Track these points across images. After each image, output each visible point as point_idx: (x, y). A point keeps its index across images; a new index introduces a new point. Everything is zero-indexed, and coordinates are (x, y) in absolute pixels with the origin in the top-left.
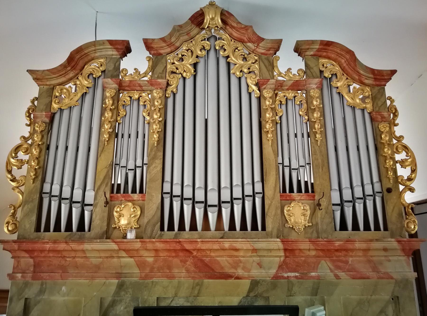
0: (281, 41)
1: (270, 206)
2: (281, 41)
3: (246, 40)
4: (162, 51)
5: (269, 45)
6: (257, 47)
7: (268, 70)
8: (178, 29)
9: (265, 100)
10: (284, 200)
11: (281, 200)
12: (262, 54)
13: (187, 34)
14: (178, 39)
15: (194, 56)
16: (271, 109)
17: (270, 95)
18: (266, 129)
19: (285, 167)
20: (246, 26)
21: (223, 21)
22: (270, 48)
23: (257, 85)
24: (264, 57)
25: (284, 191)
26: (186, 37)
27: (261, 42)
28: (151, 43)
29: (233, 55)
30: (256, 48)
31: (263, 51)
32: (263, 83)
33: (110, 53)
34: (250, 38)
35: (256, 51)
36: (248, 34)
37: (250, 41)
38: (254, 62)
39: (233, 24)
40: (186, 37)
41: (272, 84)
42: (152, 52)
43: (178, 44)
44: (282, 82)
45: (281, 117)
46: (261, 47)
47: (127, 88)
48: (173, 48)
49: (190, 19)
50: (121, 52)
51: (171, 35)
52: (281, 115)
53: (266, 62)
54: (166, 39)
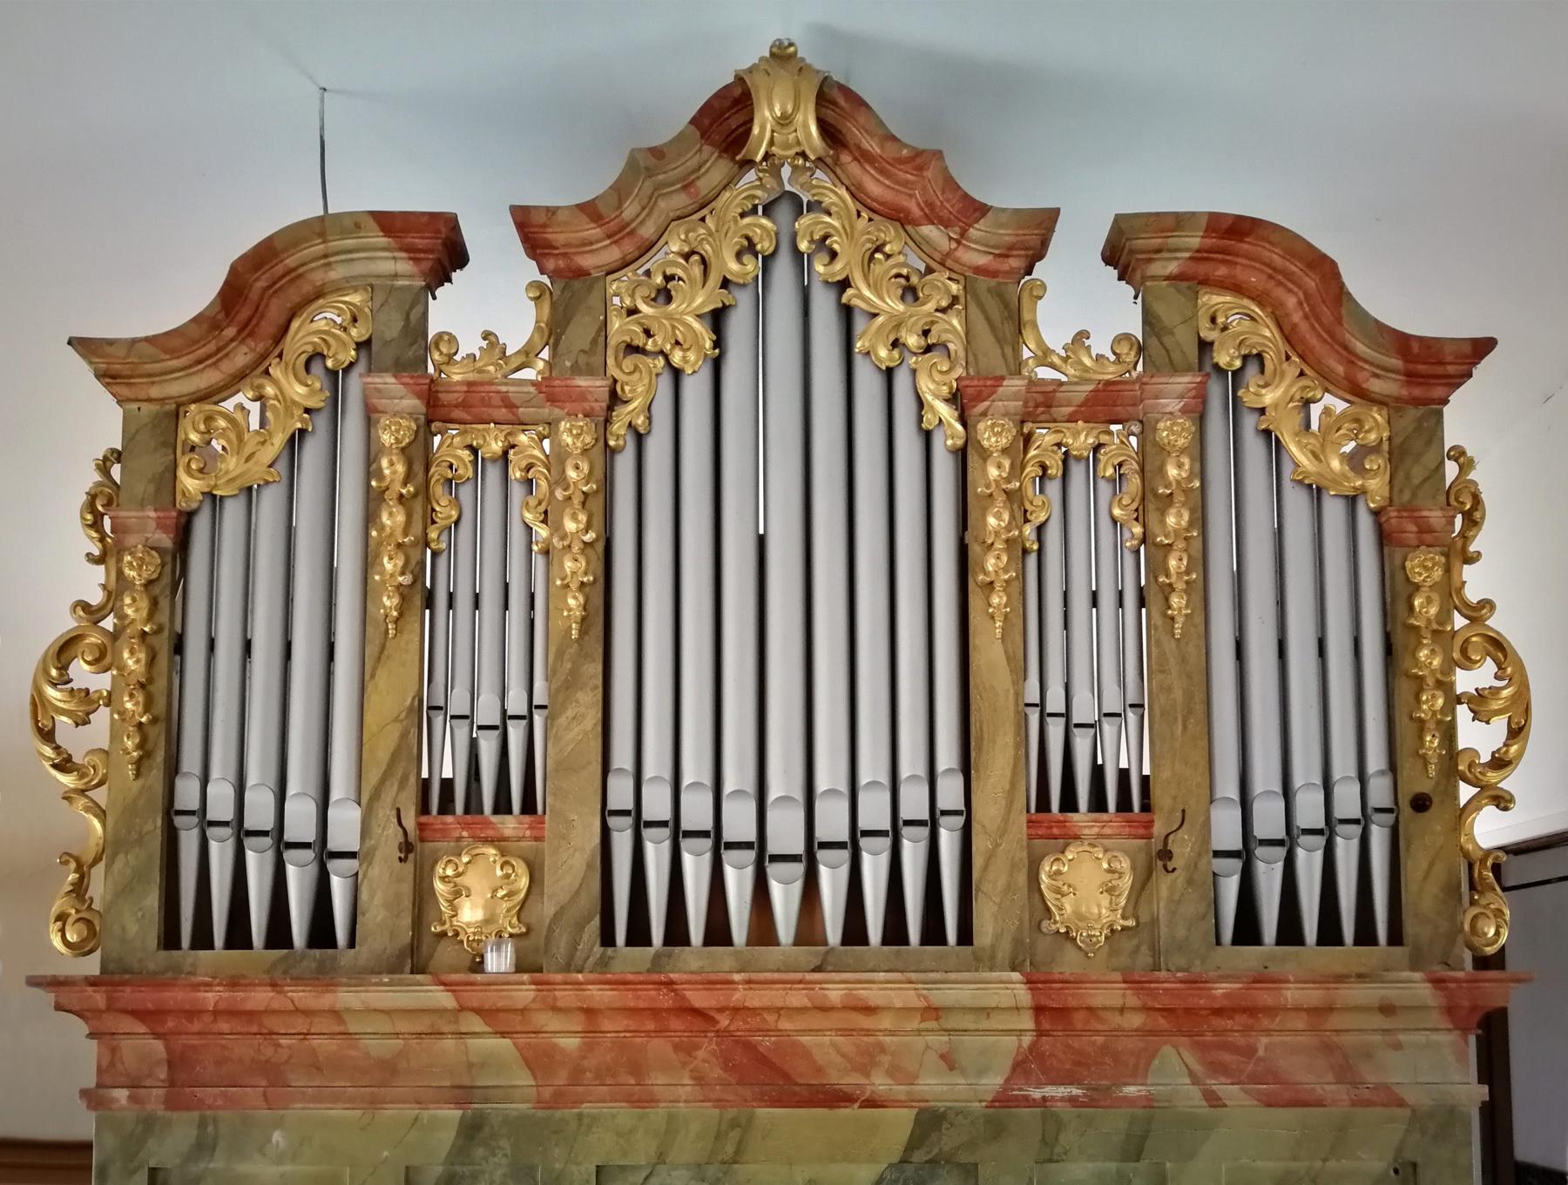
4: (587, 261)
5: (1007, 235)
6: (959, 242)
7: (998, 340)
9: (985, 460)
10: (1041, 837)
11: (1030, 837)
12: (978, 270)
13: (685, 187)
15: (714, 279)
16: (1004, 497)
17: (1004, 442)
18: (986, 573)
20: (918, 153)
22: (1011, 247)
24: (984, 283)
26: (680, 201)
27: (977, 221)
28: (544, 226)
29: (866, 277)
30: (954, 245)
31: (983, 261)
32: (980, 393)
33: (386, 267)
34: (931, 205)
36: (924, 189)
37: (932, 216)
38: (944, 303)
39: (866, 146)
41: (1014, 397)
42: (551, 264)
43: (648, 231)
44: (1050, 388)
45: (1040, 529)
48: (629, 247)
49: (694, 121)
53: (993, 305)
54: (602, 209)
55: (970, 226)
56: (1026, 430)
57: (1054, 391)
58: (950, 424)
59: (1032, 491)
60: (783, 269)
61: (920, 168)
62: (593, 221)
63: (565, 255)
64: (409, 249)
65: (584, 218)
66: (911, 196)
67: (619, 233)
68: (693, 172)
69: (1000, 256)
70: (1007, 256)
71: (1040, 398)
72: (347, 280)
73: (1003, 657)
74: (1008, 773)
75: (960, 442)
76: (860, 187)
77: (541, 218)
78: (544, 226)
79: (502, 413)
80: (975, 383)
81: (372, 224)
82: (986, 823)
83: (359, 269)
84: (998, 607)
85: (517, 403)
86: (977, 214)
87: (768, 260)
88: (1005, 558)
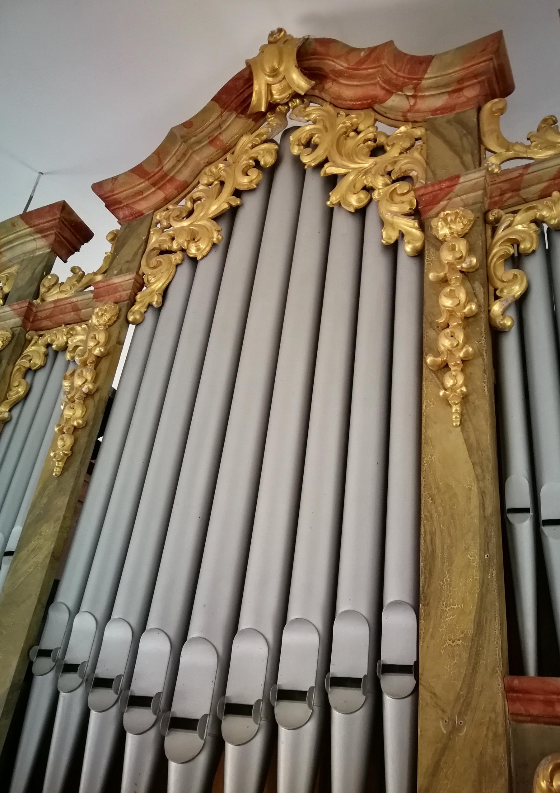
0: (498, 37)
1: (445, 747)
2: (498, 37)
3: (379, 92)
4: (143, 206)
5: (455, 71)
6: (414, 97)
7: (456, 153)
8: (184, 136)
9: (438, 249)
10: (535, 719)
11: (516, 718)
12: (435, 112)
13: (211, 142)
14: (183, 158)
15: (228, 190)
16: (459, 276)
17: (458, 227)
18: (438, 354)
19: (547, 530)
20: (372, 50)
21: (309, 72)
22: (460, 81)
23: (416, 214)
24: (441, 119)
25: (515, 663)
26: (210, 151)
27: (425, 72)
28: (112, 191)
29: (340, 153)
30: (412, 101)
31: (439, 102)
32: (435, 197)
33: (31, 246)
34: (388, 81)
35: (418, 111)
36: (383, 73)
37: (392, 88)
38: (407, 145)
39: (338, 67)
40: (210, 151)
41: (473, 189)
42: (121, 214)
43: (184, 176)
44: (516, 174)
45: (521, 304)
46: (429, 88)
47: (45, 323)
48: (170, 189)
49: (216, 99)
50: (53, 237)
51: (160, 154)
52: (517, 290)
53: (453, 133)
54: (147, 168)
55: (420, 79)
56: (491, 218)
57: (521, 175)
58: (410, 233)
59: (502, 272)
60: (285, 177)
61: (378, 59)
62: (142, 177)
63: (127, 206)
64: (40, 231)
65: (136, 177)
66: (374, 84)
67: (160, 181)
68: (215, 129)
69: (454, 91)
70: (460, 90)
71: (505, 186)
72: (10, 261)
73: (463, 448)
74: (472, 608)
75: (418, 244)
76: (339, 97)
77: (108, 187)
78: (112, 191)
79: (71, 316)
80: (430, 189)
81: (21, 222)
82: (438, 690)
83: (18, 251)
84: (453, 389)
85: (80, 308)
86: (424, 66)
87: (270, 173)
88: (461, 337)
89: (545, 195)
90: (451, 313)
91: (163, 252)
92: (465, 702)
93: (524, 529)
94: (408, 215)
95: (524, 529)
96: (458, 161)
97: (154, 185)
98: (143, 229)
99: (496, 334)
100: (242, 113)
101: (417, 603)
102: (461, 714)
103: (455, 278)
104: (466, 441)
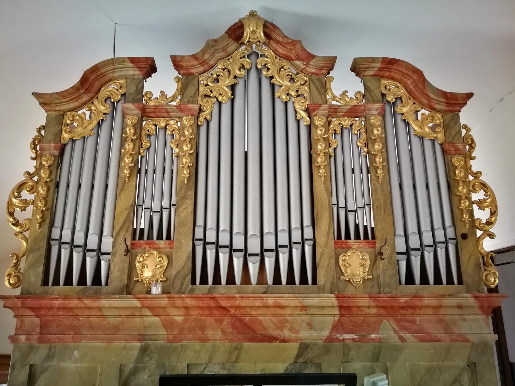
0: (335, 58)
2: (335, 58)
3: (293, 57)
4: (193, 71)
5: (321, 64)
7: (320, 93)
9: (317, 129)
10: (339, 248)
11: (335, 248)
12: (313, 73)
13: (223, 50)
17: (322, 123)
20: (294, 41)
21: (266, 35)
22: (323, 67)
24: (314, 77)
26: (222, 54)
27: (312, 60)
29: (278, 75)
30: (305, 66)
31: (314, 71)
32: (314, 109)
33: (132, 72)
34: (298, 55)
35: (306, 71)
37: (298, 58)
38: (303, 83)
39: (278, 39)
41: (325, 110)
43: (212, 62)
44: (336, 107)
45: (335, 149)
48: (206, 67)
50: (145, 72)
51: (204, 51)
53: (318, 84)
54: (198, 56)
60: (253, 74)
62: (195, 59)
63: (186, 69)
71: (333, 110)
74: (327, 227)
75: (309, 123)
78: (181, 61)
81: (128, 60)
87: (248, 71)
88: (324, 158)
89: (343, 116)
90: (321, 151)
91: (206, 96)
92: (326, 246)
93: (342, 213)
94: (304, 111)
95: (342, 213)
96: (320, 97)
97: (200, 64)
98: (195, 82)
99: (330, 156)
100: (236, 40)
101: (313, 225)
102: (326, 248)
103: (322, 140)
104: (325, 187)
